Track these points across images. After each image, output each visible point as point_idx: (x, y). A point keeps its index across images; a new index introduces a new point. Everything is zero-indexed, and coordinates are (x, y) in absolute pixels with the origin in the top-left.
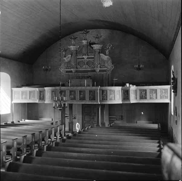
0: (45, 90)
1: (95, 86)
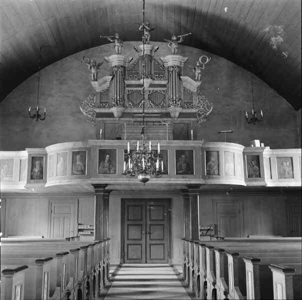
0: (47, 154)
1: (191, 139)
